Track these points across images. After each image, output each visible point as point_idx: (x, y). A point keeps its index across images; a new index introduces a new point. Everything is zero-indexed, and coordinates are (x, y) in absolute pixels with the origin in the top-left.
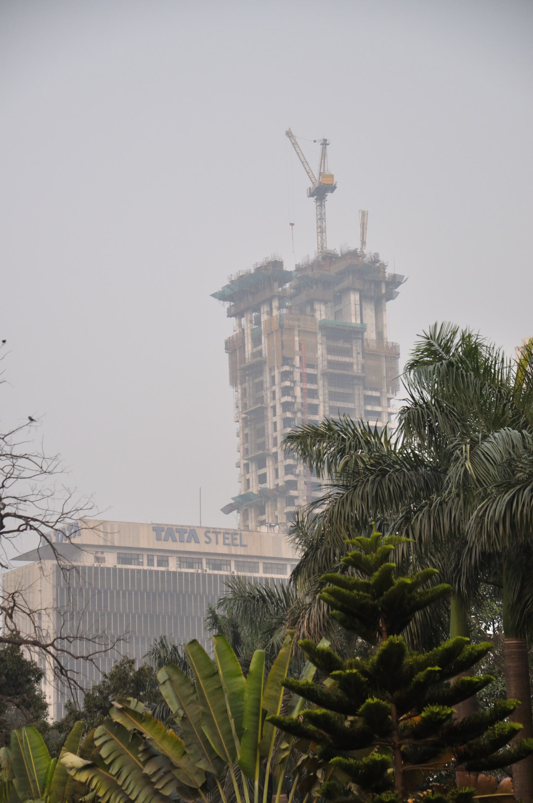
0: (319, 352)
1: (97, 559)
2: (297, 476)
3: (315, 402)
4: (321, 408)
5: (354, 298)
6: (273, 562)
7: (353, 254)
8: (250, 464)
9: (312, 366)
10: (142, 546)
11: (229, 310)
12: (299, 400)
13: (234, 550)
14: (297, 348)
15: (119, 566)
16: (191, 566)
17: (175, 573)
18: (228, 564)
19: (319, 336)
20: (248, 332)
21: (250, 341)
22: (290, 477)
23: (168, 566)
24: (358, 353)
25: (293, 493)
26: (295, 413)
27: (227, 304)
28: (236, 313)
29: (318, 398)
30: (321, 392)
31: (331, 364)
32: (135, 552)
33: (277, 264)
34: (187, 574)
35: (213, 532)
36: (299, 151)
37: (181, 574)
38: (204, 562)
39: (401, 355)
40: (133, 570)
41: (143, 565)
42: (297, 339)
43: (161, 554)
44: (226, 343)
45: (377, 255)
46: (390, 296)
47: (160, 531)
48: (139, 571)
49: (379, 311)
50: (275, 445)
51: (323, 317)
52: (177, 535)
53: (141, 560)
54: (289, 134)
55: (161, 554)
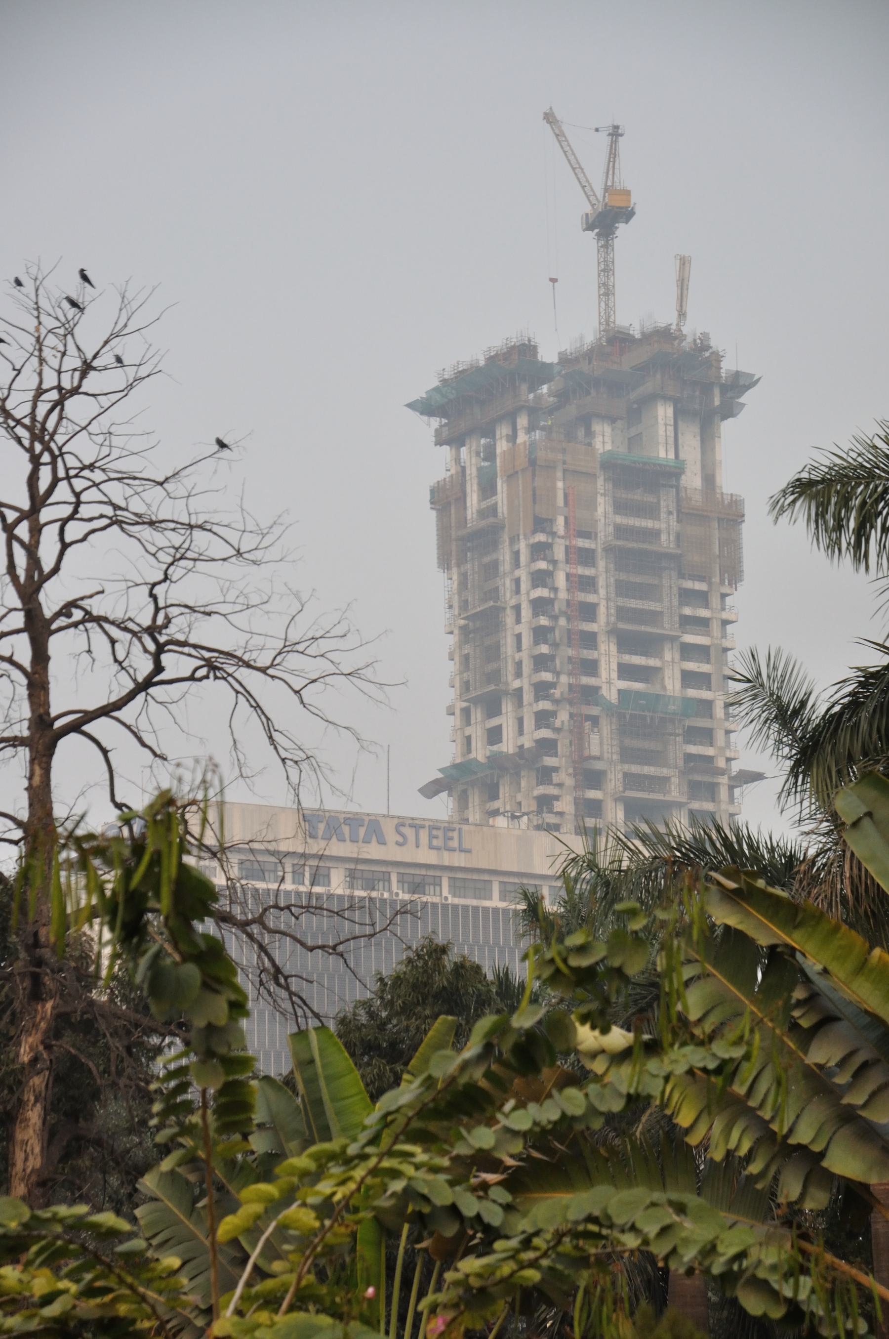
0: (600, 510)
2: (558, 730)
3: (591, 598)
4: (602, 610)
5: (664, 412)
8: (473, 710)
12: (563, 595)
13: (447, 859)
14: (560, 502)
19: (600, 482)
21: (475, 487)
23: (329, 884)
24: (670, 513)
25: (549, 761)
27: (435, 422)
28: (451, 439)
29: (596, 592)
30: (601, 582)
31: (621, 531)
35: (411, 826)
39: (746, 518)
42: (560, 485)
45: (705, 336)
49: (708, 437)
50: (519, 674)
51: (608, 447)
52: (346, 829)
54: (550, 118)
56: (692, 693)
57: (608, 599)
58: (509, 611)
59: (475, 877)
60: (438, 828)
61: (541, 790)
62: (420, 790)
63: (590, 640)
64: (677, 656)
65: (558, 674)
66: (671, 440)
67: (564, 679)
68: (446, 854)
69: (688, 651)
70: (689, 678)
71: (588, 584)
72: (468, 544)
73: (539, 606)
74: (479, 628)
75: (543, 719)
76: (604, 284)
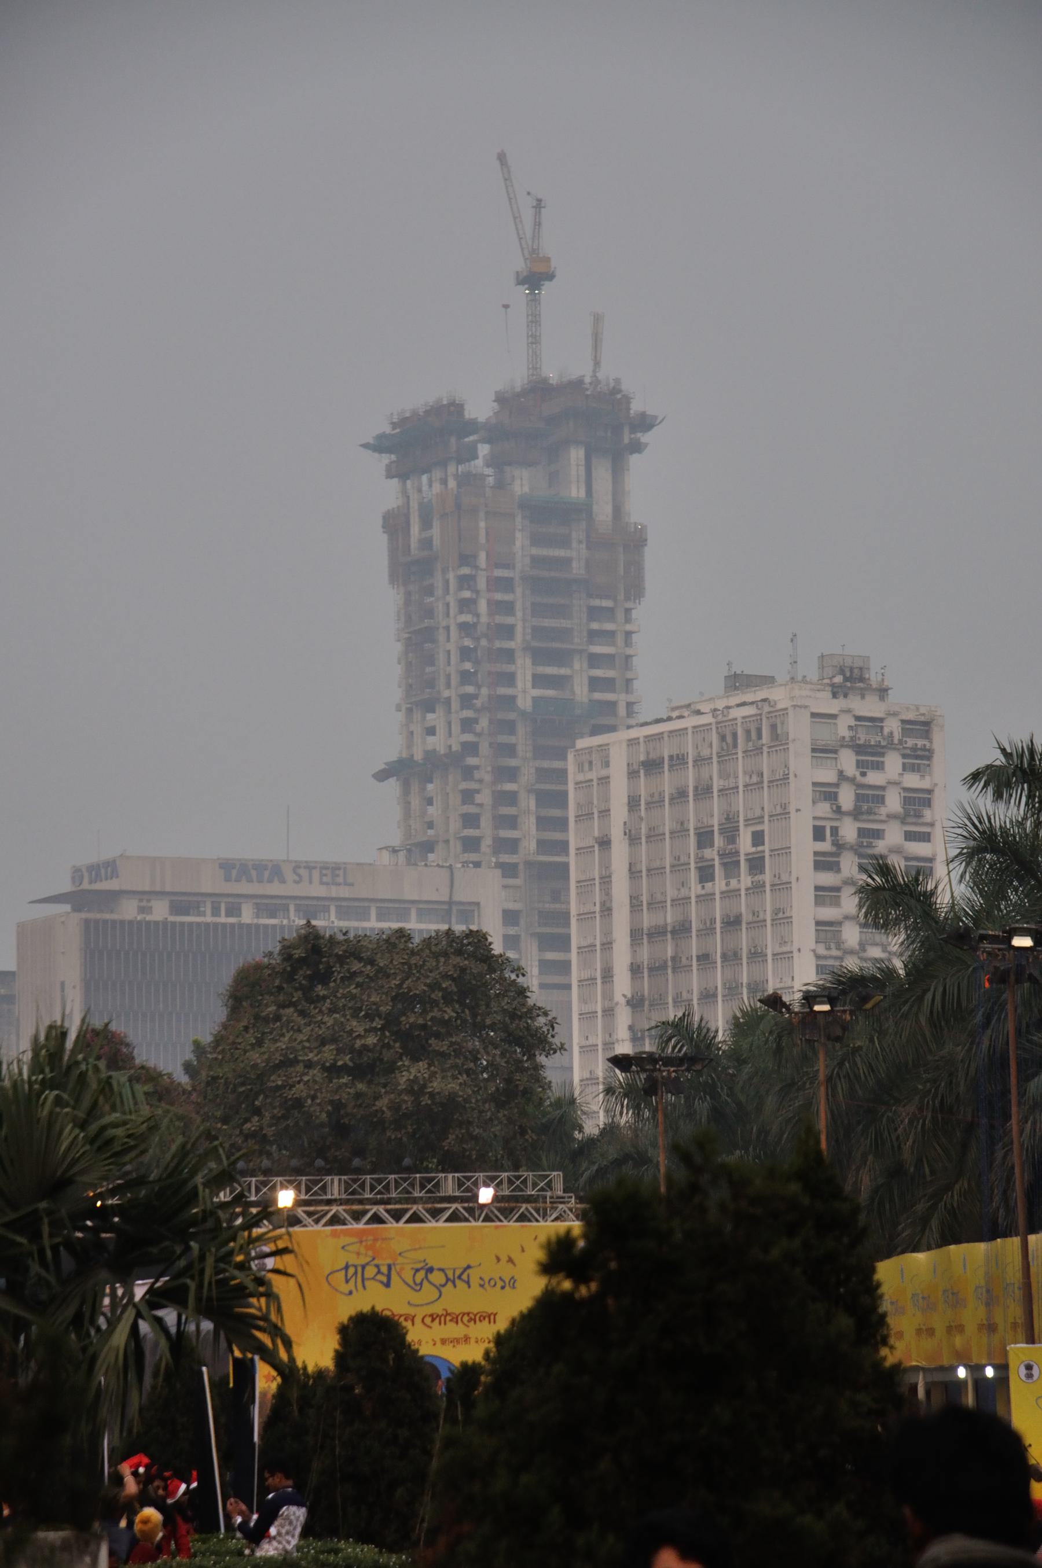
0: (518, 543)
1: (142, 910)
2: (479, 735)
3: (509, 620)
4: (519, 630)
5: (576, 455)
6: (391, 905)
7: (577, 385)
8: (415, 710)
9: (506, 566)
10: (203, 891)
11: (388, 468)
12: (484, 619)
13: (334, 892)
14: (482, 539)
15: (171, 918)
16: (273, 915)
17: (249, 926)
18: (326, 909)
19: (518, 519)
20: (414, 505)
21: (417, 519)
22: (468, 737)
23: (240, 916)
24: (580, 542)
25: (471, 761)
26: (477, 640)
27: (386, 459)
28: (400, 472)
29: (514, 615)
30: (518, 606)
31: (536, 561)
32: (195, 899)
33: (456, 408)
34: (266, 926)
35: (305, 867)
36: (512, 196)
37: (257, 926)
38: (292, 908)
39: (649, 542)
40: (191, 924)
41: (205, 916)
42: (482, 524)
43: (230, 900)
44: (384, 518)
45: (617, 381)
46: (637, 447)
47: (229, 868)
48: (198, 924)
49: (618, 470)
50: (448, 686)
51: (526, 489)
52: (254, 873)
53: (202, 909)
54: (502, 158)
55: (230, 900)
56: (598, 696)
57: (524, 620)
58: (441, 631)
59: (357, 904)
60: (327, 868)
61: (463, 785)
62: (374, 776)
63: (509, 655)
64: (585, 665)
65: (479, 687)
66: (583, 478)
67: (484, 691)
68: (333, 888)
69: (594, 660)
70: (595, 684)
71: (509, 608)
72: (411, 570)
73: (464, 627)
74: (419, 641)
75: (467, 725)
76: (532, 336)
